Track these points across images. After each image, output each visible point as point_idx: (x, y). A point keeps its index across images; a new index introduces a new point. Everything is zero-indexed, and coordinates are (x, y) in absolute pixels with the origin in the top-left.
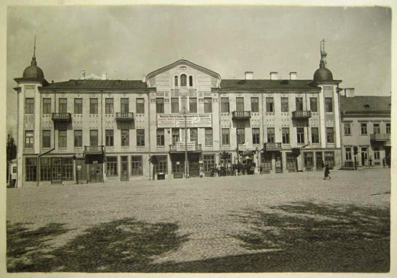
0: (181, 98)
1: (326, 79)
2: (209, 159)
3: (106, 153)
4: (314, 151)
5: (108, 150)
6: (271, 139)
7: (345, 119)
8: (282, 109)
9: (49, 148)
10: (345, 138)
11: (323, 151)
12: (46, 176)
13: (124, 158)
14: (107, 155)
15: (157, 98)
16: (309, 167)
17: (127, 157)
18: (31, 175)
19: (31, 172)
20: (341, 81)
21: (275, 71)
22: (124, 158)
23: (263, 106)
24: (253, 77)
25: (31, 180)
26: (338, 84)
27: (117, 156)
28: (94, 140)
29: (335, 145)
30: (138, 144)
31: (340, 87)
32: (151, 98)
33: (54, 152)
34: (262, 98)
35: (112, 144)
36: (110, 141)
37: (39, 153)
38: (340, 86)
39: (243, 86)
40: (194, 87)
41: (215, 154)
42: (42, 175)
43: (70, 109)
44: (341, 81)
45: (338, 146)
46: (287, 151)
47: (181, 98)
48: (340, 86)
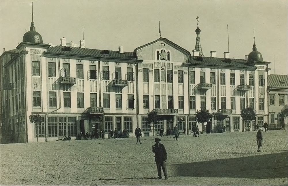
2: (193, 120)
3: (105, 114)
5: (106, 111)
6: (223, 105)
8: (179, 80)
11: (122, 116)
14: (106, 115)
17: (120, 117)
19: (53, 131)
20: (270, 63)
21: (215, 51)
22: (119, 119)
23: (218, 78)
25: (53, 136)
26: (267, 65)
28: (158, 104)
30: (117, 107)
32: (190, 71)
33: (58, 111)
34: (218, 72)
35: (109, 107)
36: (107, 104)
37: (47, 112)
38: (269, 66)
39: (228, 64)
40: (171, 61)
41: (264, 117)
43: (73, 74)
44: (270, 63)
45: (267, 113)
46: (124, 116)
48: (269, 66)
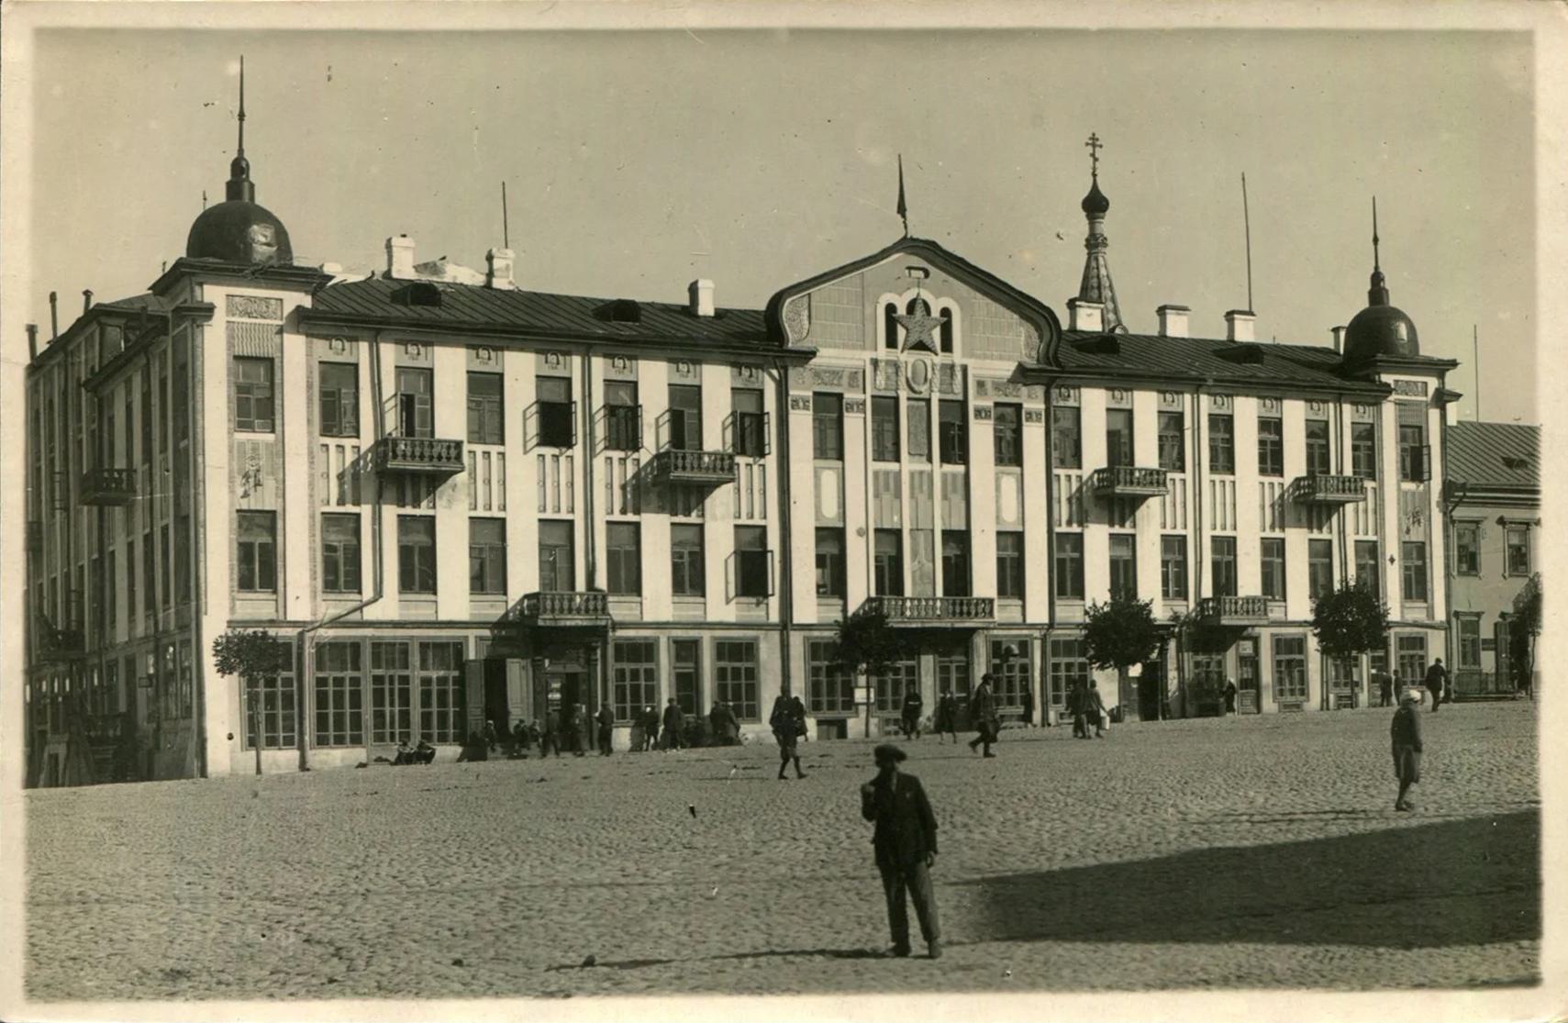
0: (909, 399)
1: (1168, 311)
3: (616, 626)
4: (663, 638)
5: (619, 609)
6: (1225, 575)
7: (1460, 513)
9: (352, 596)
10: (1460, 583)
12: (339, 725)
13: (687, 650)
14: (620, 633)
15: (997, 405)
16: (1289, 699)
18: (443, 717)
20: (1453, 364)
22: (687, 650)
24: (1256, 333)
25: (340, 741)
26: (1441, 376)
27: (657, 639)
28: (889, 573)
29: (1430, 612)
30: (678, 587)
31: (1448, 387)
32: (1054, 403)
33: (371, 613)
34: (1198, 408)
35: (636, 588)
36: (627, 574)
42: (426, 718)
44: (1453, 364)
45: (1440, 615)
47: (909, 399)
